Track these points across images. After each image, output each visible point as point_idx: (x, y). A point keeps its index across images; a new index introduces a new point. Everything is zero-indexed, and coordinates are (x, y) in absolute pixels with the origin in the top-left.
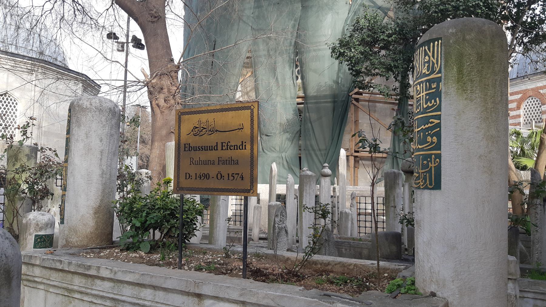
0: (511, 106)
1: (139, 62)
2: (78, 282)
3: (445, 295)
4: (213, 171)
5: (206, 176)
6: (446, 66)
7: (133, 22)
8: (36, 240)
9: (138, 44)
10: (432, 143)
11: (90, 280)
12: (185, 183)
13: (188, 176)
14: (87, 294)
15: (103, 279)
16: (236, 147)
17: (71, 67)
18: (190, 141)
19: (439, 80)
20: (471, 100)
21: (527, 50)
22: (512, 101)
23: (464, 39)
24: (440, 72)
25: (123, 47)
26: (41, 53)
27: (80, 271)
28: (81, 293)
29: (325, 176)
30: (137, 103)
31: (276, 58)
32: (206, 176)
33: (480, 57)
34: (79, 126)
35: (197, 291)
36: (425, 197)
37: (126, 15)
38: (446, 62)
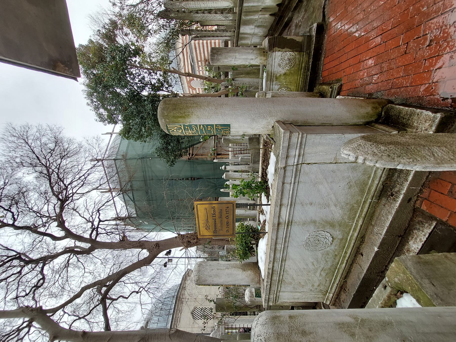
0: (195, 93)
1: (177, 252)
2: (275, 278)
3: (273, 122)
4: (225, 220)
5: (228, 223)
6: (178, 123)
7: (159, 256)
8: (258, 297)
9: (169, 253)
10: (211, 128)
11: (274, 272)
12: (231, 232)
13: (228, 231)
14: (280, 273)
15: (273, 267)
16: (214, 211)
17: (180, 283)
18: (212, 231)
19: (184, 126)
20: (193, 112)
21: (171, 86)
22: (193, 92)
23: (167, 116)
24: (181, 125)
25: (170, 260)
26: (173, 297)
27: (270, 277)
28: (279, 276)
29: (225, 168)
30: (195, 252)
31: (142, 52)
32: (228, 223)
33: (175, 109)
34: (206, 280)
35: (277, 225)
36: (233, 131)
37: (156, 259)
38: (176, 123)
